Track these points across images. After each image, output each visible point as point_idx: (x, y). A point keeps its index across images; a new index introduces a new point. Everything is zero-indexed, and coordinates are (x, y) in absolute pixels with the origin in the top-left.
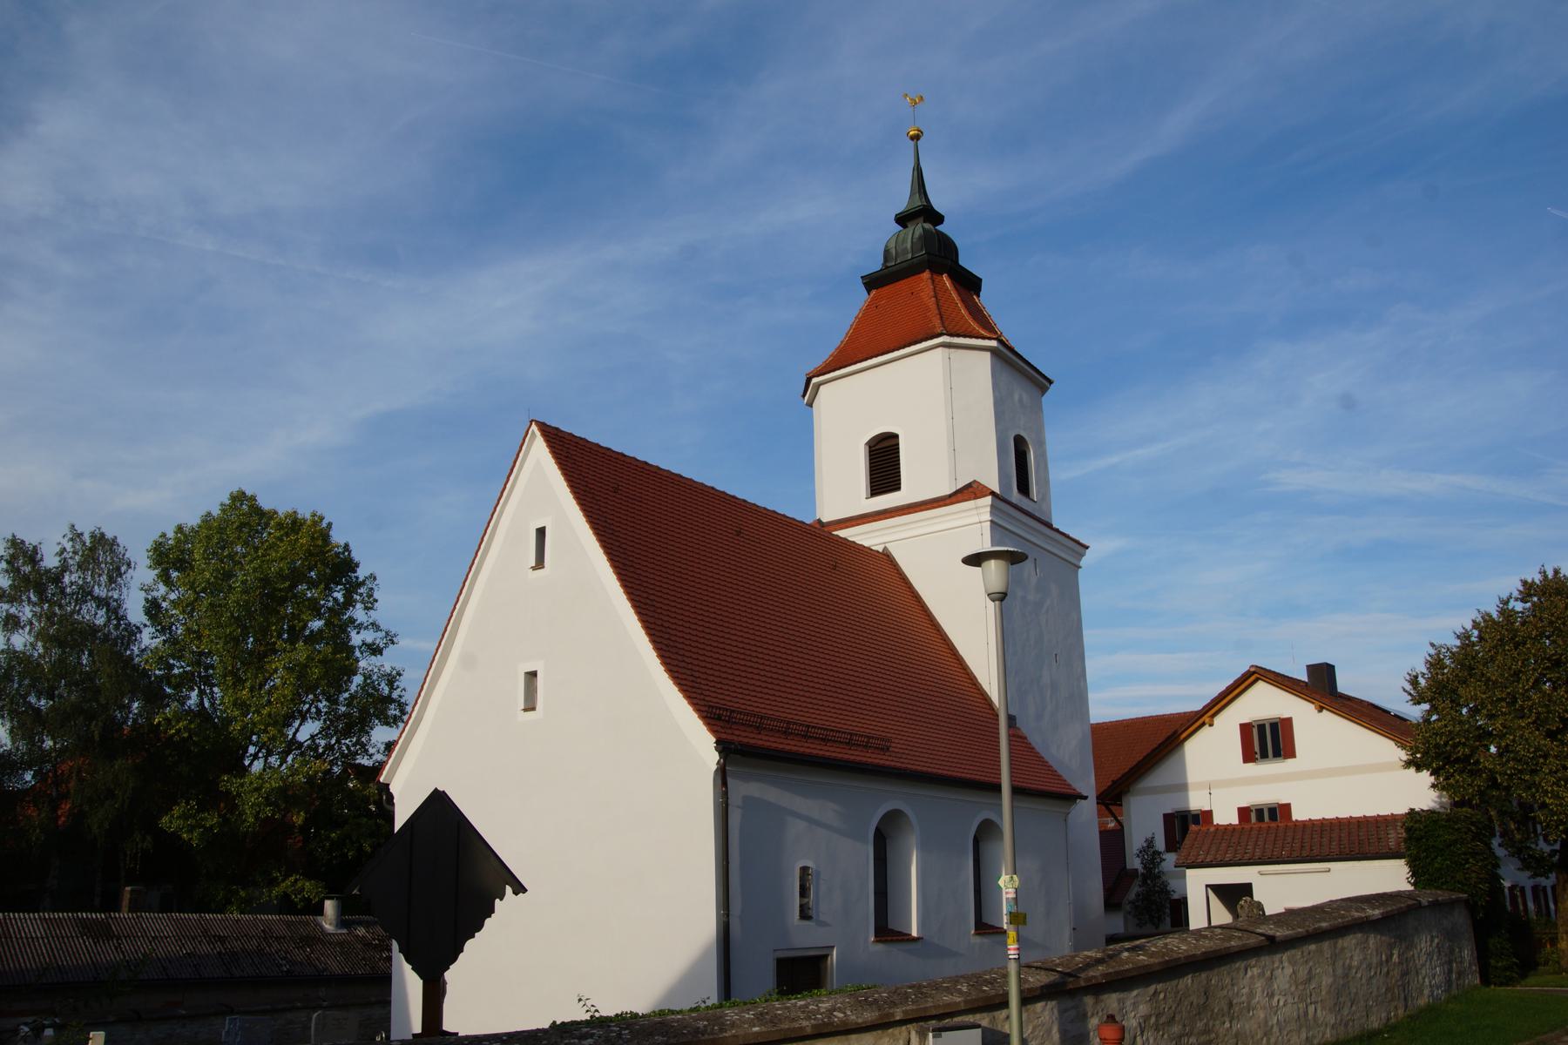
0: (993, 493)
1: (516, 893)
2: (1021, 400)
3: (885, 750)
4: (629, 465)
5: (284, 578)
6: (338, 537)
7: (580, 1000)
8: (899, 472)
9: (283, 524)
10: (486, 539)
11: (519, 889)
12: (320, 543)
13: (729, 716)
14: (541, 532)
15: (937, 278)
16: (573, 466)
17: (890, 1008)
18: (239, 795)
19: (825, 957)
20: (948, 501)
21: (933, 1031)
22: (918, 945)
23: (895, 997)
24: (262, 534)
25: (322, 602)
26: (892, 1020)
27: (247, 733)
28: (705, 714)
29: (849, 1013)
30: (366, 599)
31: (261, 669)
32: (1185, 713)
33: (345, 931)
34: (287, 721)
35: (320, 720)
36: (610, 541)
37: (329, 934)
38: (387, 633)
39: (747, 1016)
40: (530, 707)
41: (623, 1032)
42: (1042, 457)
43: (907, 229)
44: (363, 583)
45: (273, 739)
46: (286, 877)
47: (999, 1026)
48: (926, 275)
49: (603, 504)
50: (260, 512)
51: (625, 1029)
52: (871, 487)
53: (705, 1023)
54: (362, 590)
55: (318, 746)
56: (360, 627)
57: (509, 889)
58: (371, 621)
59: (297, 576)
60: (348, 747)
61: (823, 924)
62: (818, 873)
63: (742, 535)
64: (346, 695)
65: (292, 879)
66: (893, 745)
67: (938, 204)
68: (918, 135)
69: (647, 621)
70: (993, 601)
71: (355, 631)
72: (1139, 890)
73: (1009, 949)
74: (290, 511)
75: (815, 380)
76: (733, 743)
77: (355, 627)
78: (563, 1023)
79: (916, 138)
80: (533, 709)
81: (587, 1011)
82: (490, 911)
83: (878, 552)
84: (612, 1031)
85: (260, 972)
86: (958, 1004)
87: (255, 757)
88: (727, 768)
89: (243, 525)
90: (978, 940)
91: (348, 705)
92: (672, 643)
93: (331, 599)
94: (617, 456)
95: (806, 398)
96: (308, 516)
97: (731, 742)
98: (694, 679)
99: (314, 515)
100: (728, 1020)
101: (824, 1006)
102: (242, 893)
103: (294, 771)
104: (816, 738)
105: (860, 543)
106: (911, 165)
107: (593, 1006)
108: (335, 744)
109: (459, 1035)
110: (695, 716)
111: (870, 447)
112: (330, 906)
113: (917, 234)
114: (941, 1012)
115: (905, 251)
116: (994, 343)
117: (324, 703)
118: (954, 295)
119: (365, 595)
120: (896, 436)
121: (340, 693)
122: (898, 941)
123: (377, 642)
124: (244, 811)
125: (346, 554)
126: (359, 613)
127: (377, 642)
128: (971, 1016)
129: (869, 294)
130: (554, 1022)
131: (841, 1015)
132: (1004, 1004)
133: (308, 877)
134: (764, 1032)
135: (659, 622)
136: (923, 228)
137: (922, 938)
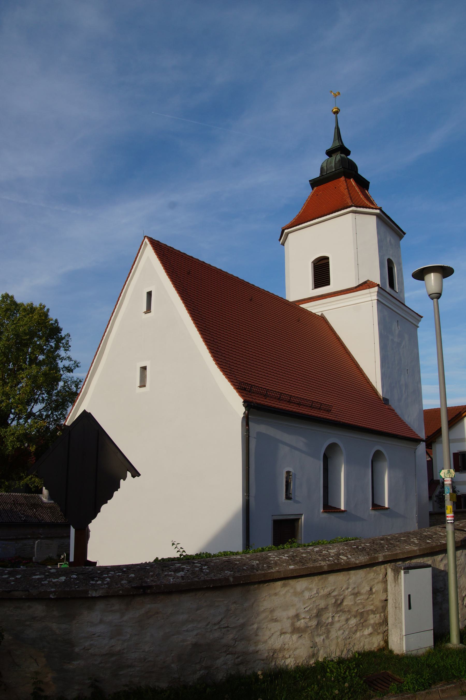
0: (378, 285)
1: (133, 476)
2: (390, 241)
3: (329, 411)
4: (195, 262)
5: (26, 334)
6: (52, 315)
7: (173, 544)
8: (329, 276)
9: (26, 309)
10: (121, 298)
11: (136, 474)
12: (43, 318)
13: (250, 389)
14: (149, 294)
15: (348, 181)
16: (167, 259)
17: (375, 553)
18: (5, 437)
19: (298, 520)
20: (355, 290)
21: (404, 569)
22: (387, 512)
23: (375, 546)
24: (17, 314)
25: (45, 347)
26: (377, 561)
27: (9, 407)
28: (237, 387)
29: (350, 557)
30: (65, 345)
31: (15, 377)
32: (455, 407)
33: (52, 502)
34: (28, 403)
35: (43, 403)
36: (186, 297)
37: (45, 503)
38: (75, 362)
39: (284, 558)
40: (143, 385)
41: (204, 567)
42: (400, 271)
43: (332, 158)
44: (64, 338)
45: (20, 410)
46: (27, 476)
47: (437, 565)
48: (343, 179)
49: (182, 279)
50: (14, 303)
51: (205, 565)
52: (315, 284)
53: (257, 562)
54: (63, 341)
55: (42, 415)
56: (62, 359)
57: (129, 474)
58: (67, 356)
59: (32, 334)
60: (57, 416)
61: (298, 502)
62: (295, 475)
63: (252, 301)
64: (55, 391)
65: (30, 477)
66: (332, 409)
67: (347, 145)
68: (337, 111)
69: (206, 338)
70: (432, 299)
71: (60, 361)
72: (441, 490)
73: (447, 517)
74: (30, 303)
75: (286, 231)
76: (253, 403)
77: (60, 359)
78: (163, 559)
79: (336, 113)
80: (144, 386)
81: (178, 551)
82: (117, 487)
83: (319, 315)
84: (196, 567)
85: (11, 521)
86: (414, 551)
87: (13, 420)
88: (249, 417)
89: (7, 310)
90: (373, 512)
91: (56, 396)
92: (219, 350)
93: (49, 346)
94: (189, 258)
95: (281, 241)
96: (38, 306)
97: (251, 402)
98: (231, 369)
99: (41, 305)
100: (272, 560)
101: (333, 551)
102: (6, 483)
103: (31, 426)
104: (294, 403)
105: (310, 311)
106: (334, 125)
107: (181, 548)
108: (50, 414)
109: (97, 565)
110: (231, 388)
111: (314, 264)
112: (45, 491)
113: (337, 160)
114: (406, 556)
115: (331, 168)
116: (378, 211)
117: (46, 395)
118: (357, 189)
119: (65, 343)
120: (327, 258)
121: (53, 391)
122: (334, 512)
123: (71, 366)
124: (7, 444)
125: (56, 324)
126: (62, 352)
127: (71, 366)
128: (421, 559)
129: (313, 189)
130: (157, 558)
131: (345, 558)
132: (443, 550)
133: (37, 476)
134: (297, 569)
135: (212, 339)
136: (341, 156)
137: (347, 511)
